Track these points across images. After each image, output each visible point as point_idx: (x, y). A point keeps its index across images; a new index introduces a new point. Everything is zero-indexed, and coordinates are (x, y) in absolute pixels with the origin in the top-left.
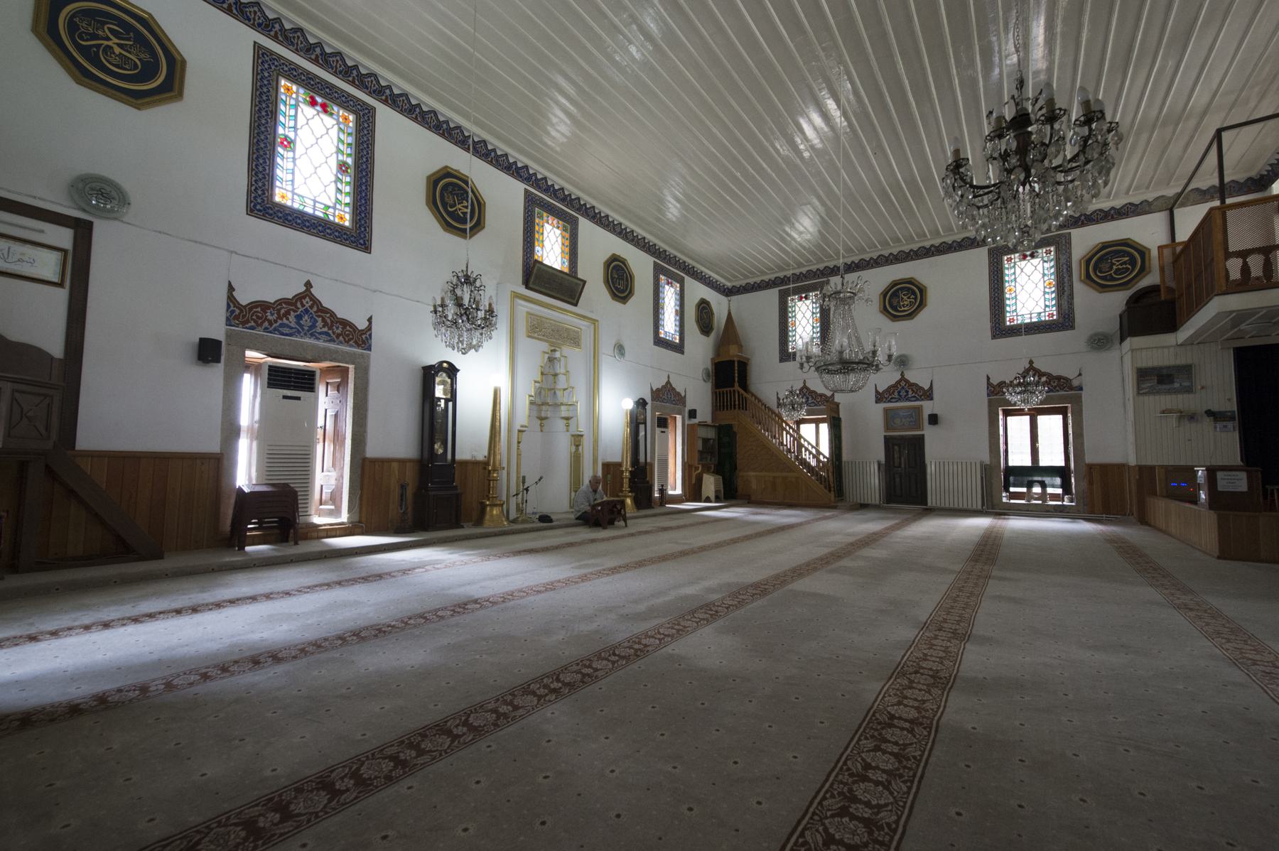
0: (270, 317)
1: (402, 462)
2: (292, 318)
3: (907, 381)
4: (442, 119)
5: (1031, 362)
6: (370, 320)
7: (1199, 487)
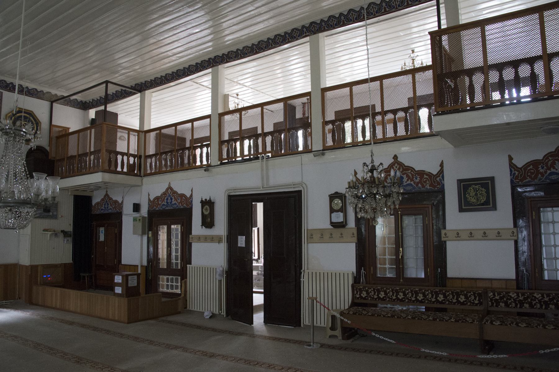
0: (542, 170)
5: (395, 157)
6: (442, 165)
7: (402, 309)
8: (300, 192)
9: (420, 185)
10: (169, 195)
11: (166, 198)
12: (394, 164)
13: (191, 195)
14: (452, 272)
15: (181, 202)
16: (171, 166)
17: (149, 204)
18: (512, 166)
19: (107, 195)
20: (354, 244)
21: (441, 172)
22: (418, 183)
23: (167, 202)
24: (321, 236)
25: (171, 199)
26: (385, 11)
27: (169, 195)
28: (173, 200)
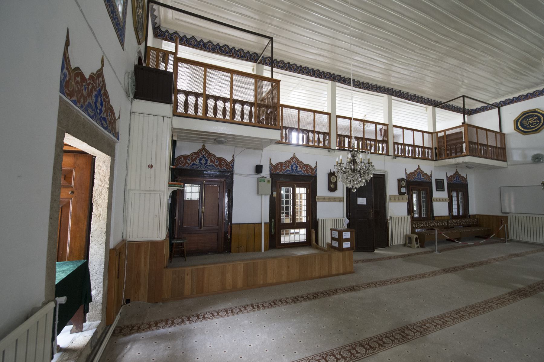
0: (188, 162)
1: (154, 245)
2: (197, 161)
3: (207, 151)
4: (245, 52)
5: (419, 166)
8: (384, 176)
9: (219, 167)
10: (203, 156)
11: (290, 165)
12: (202, 150)
13: (316, 167)
14: (435, 215)
15: (306, 170)
16: (362, 149)
17: (270, 168)
18: (271, 164)
19: (457, 172)
20: (406, 203)
21: (431, 175)
22: (217, 166)
23: (292, 169)
24: (394, 199)
25: (297, 167)
26: (184, 43)
27: (294, 164)
28: (299, 168)
